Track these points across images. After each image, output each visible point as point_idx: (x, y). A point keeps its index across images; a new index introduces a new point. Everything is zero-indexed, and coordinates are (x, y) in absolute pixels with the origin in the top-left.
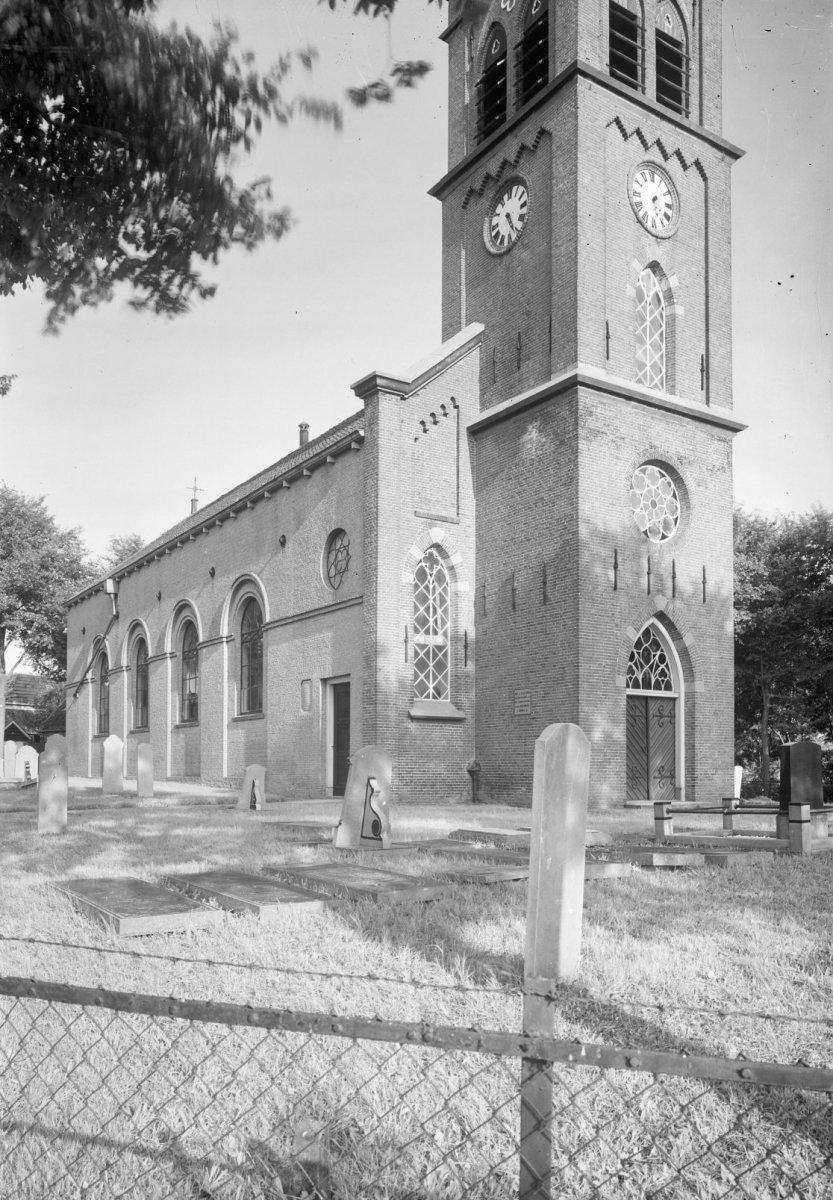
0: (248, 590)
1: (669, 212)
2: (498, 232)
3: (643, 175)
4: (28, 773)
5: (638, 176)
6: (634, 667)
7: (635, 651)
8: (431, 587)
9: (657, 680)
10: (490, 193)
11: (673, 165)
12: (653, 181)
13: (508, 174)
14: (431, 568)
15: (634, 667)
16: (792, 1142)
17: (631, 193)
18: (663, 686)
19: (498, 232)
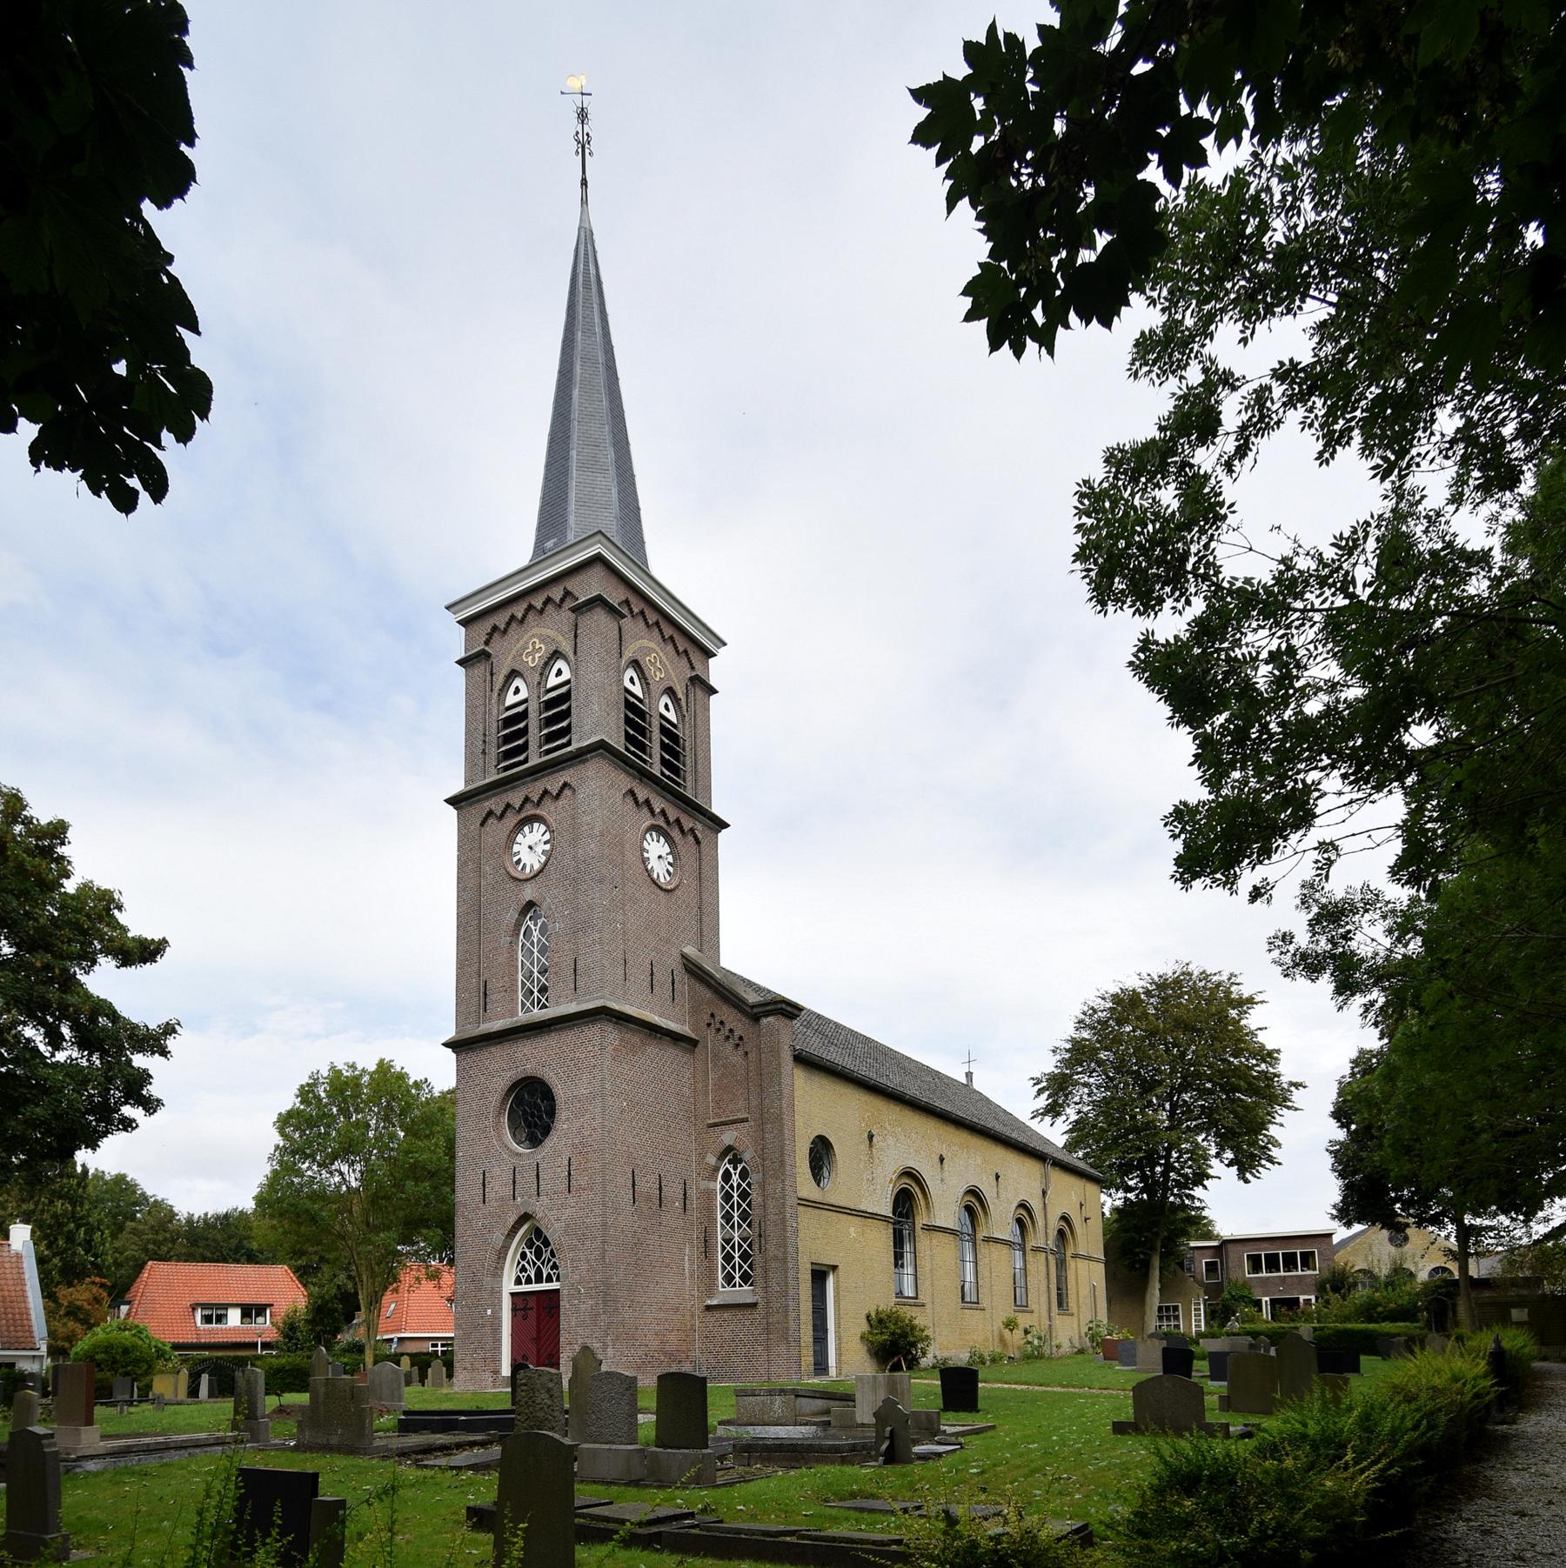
0: (907, 1181)
1: (671, 869)
2: (520, 859)
3: (651, 835)
4: (1209, 1394)
5: (648, 836)
6: (526, 1265)
7: (527, 1251)
8: (735, 1185)
9: (549, 1274)
10: (511, 820)
11: (675, 834)
12: (658, 841)
13: (530, 810)
14: (735, 1168)
15: (526, 1265)
16: (1453, 1557)
17: (643, 850)
18: (523, 1281)
19: (520, 859)
